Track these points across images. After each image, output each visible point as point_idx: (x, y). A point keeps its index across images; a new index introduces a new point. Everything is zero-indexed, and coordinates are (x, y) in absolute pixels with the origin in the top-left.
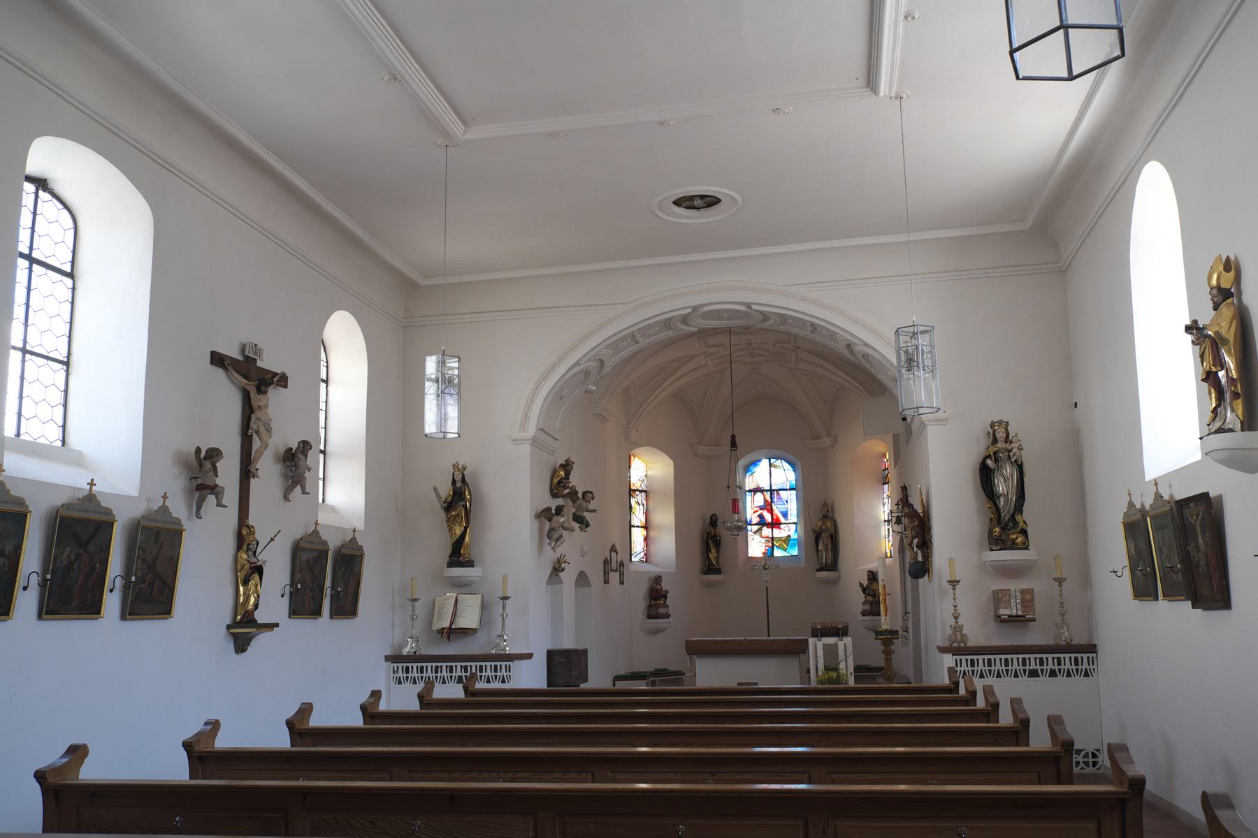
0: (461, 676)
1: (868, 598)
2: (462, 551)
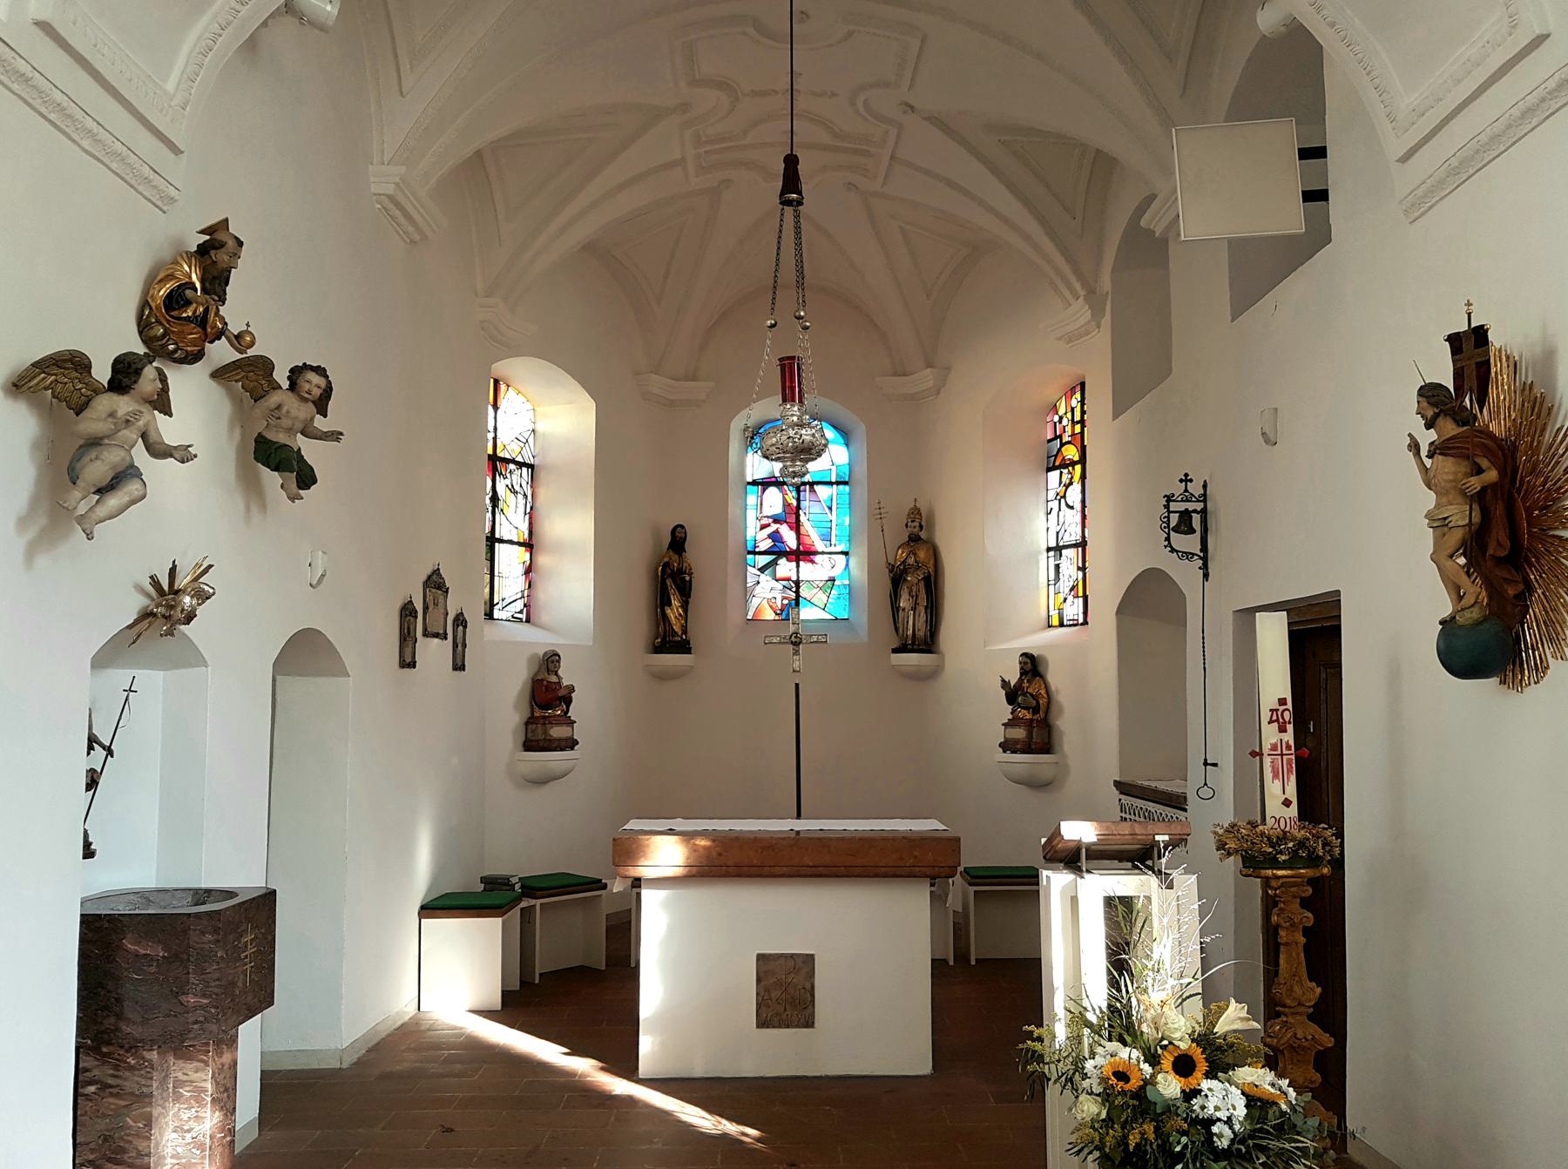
1: (1022, 713)
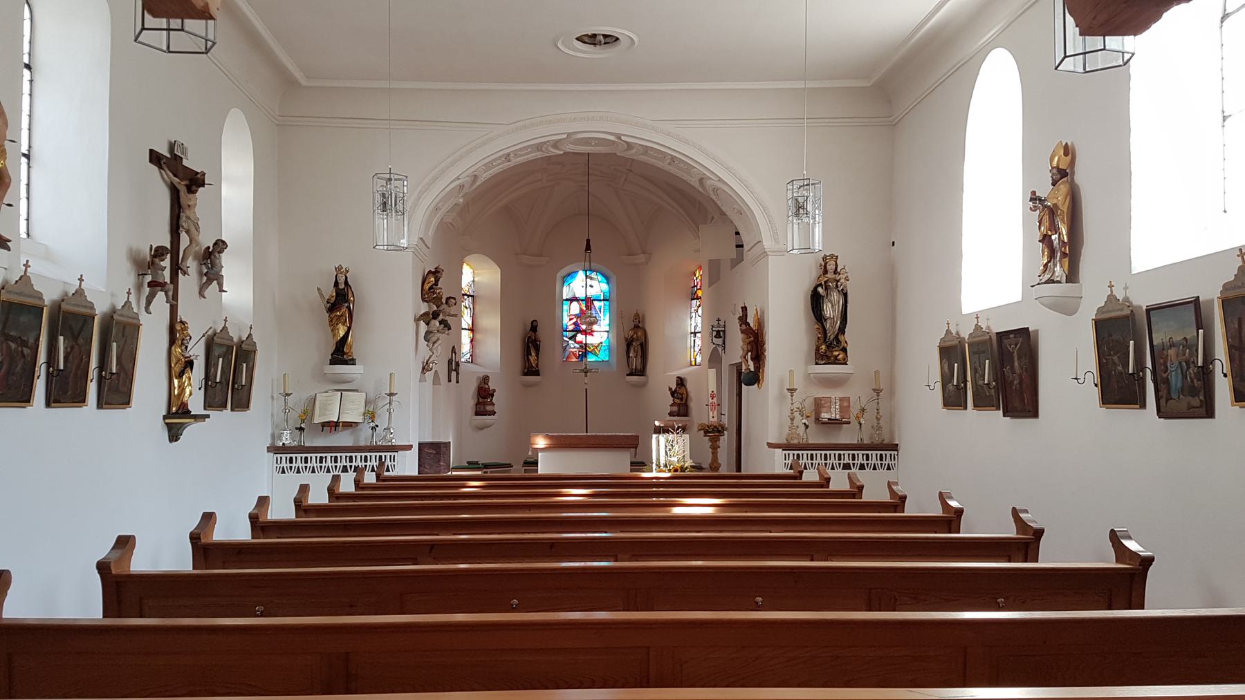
0: (346, 466)
1: (676, 401)
2: (345, 350)
